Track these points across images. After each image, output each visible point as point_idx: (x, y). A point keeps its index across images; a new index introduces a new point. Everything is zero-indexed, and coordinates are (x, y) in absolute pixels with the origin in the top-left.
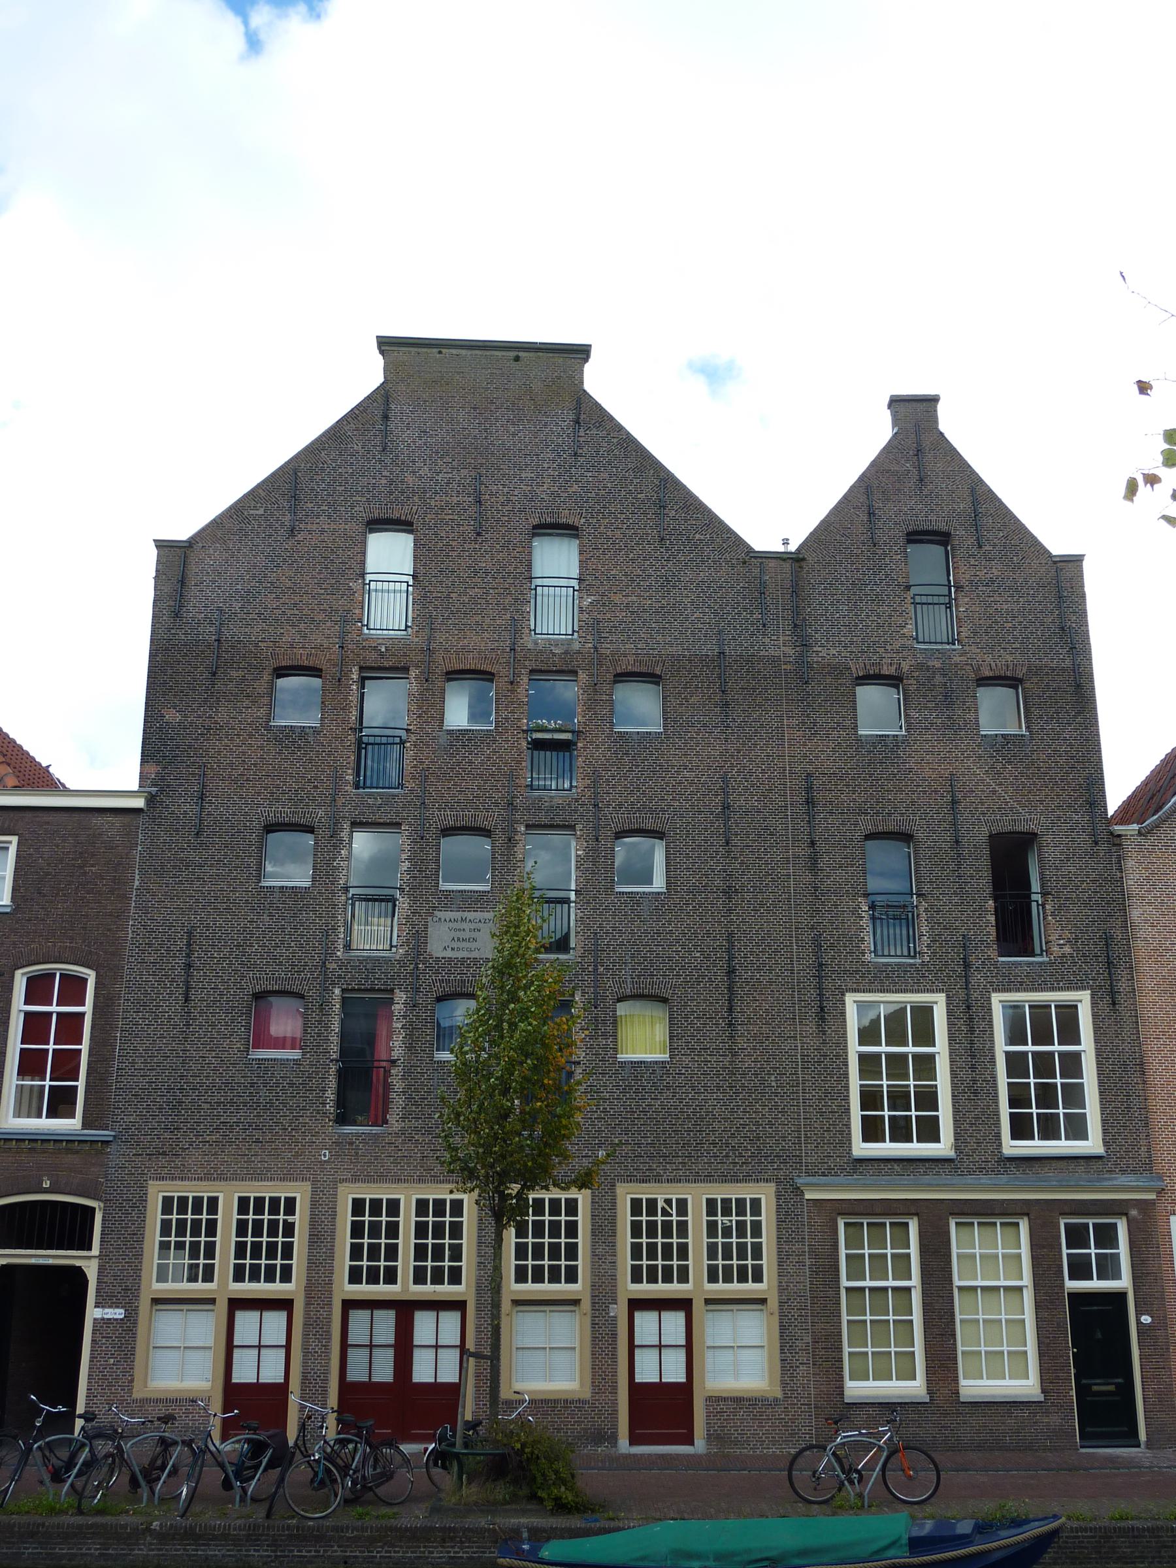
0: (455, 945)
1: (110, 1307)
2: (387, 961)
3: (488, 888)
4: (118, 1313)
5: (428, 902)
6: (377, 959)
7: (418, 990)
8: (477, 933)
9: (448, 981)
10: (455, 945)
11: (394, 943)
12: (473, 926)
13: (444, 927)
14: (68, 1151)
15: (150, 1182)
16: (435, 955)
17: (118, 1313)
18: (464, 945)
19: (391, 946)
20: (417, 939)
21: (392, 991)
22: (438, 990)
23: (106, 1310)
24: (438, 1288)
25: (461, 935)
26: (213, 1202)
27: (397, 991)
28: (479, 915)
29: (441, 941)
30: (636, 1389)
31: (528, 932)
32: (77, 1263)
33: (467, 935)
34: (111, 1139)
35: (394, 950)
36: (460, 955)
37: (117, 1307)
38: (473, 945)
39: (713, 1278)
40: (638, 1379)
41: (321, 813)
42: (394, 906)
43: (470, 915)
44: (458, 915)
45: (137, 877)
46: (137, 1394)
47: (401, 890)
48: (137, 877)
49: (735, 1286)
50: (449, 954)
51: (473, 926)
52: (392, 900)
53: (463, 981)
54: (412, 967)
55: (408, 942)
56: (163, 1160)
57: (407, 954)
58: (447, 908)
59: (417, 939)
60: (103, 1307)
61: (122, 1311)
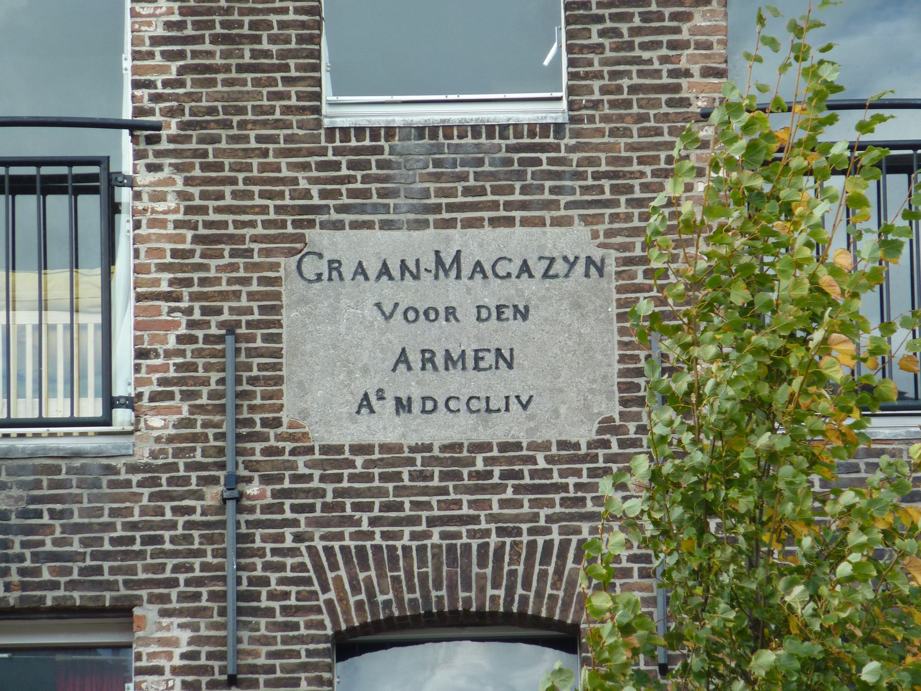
0: (413, 385)
2: (99, 472)
3: (557, 112)
5: (272, 185)
6: (48, 465)
7: (246, 606)
8: (516, 325)
9: (387, 559)
10: (413, 385)
11: (122, 387)
12: (492, 293)
13: (357, 304)
16: (321, 434)
18: (456, 383)
19: (111, 403)
20: (230, 358)
21: (122, 612)
22: (345, 600)
24: (129, 72)
25: (437, 336)
27: (147, 612)
28: (518, 241)
29: (348, 362)
31: (816, 303)
33: (465, 336)
35: (122, 417)
36: (439, 431)
38: (495, 384)
41: (156, 421)
42: (112, 209)
43: (479, 243)
44: (419, 244)
47: (143, 130)
50: (385, 428)
51: (492, 293)
52: (93, 181)
53: (455, 555)
54: (212, 494)
55: (186, 382)
57: (185, 438)
58: (362, 213)
59: (230, 358)
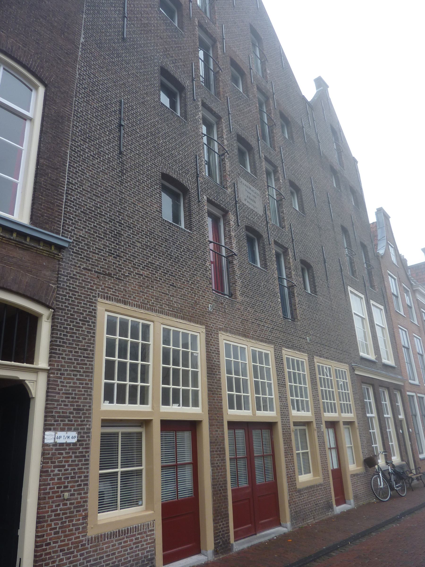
1: (62, 430)
4: (69, 437)
14: (19, 245)
15: (99, 299)
17: (69, 437)
23: (59, 434)
26: (146, 328)
30: (44, 445)
32: (21, 376)
34: (66, 245)
37: (69, 430)
39: (166, 402)
40: (46, 441)
45: (83, 36)
46: (91, 533)
48: (83, 32)
49: (127, 407)
56: (109, 282)
60: (55, 430)
61: (75, 434)
